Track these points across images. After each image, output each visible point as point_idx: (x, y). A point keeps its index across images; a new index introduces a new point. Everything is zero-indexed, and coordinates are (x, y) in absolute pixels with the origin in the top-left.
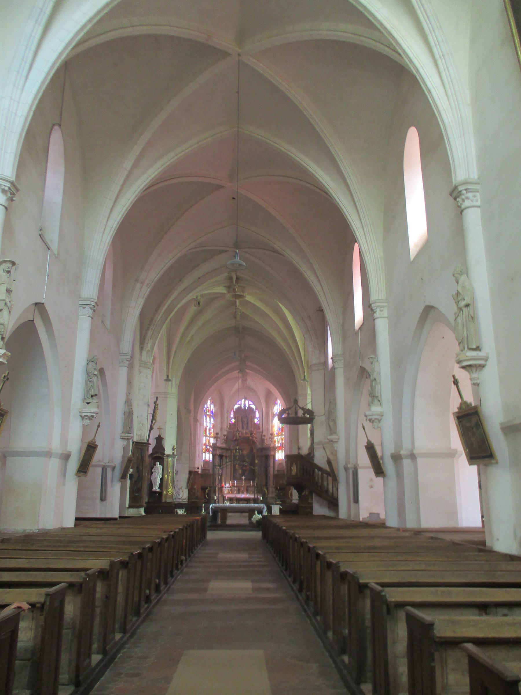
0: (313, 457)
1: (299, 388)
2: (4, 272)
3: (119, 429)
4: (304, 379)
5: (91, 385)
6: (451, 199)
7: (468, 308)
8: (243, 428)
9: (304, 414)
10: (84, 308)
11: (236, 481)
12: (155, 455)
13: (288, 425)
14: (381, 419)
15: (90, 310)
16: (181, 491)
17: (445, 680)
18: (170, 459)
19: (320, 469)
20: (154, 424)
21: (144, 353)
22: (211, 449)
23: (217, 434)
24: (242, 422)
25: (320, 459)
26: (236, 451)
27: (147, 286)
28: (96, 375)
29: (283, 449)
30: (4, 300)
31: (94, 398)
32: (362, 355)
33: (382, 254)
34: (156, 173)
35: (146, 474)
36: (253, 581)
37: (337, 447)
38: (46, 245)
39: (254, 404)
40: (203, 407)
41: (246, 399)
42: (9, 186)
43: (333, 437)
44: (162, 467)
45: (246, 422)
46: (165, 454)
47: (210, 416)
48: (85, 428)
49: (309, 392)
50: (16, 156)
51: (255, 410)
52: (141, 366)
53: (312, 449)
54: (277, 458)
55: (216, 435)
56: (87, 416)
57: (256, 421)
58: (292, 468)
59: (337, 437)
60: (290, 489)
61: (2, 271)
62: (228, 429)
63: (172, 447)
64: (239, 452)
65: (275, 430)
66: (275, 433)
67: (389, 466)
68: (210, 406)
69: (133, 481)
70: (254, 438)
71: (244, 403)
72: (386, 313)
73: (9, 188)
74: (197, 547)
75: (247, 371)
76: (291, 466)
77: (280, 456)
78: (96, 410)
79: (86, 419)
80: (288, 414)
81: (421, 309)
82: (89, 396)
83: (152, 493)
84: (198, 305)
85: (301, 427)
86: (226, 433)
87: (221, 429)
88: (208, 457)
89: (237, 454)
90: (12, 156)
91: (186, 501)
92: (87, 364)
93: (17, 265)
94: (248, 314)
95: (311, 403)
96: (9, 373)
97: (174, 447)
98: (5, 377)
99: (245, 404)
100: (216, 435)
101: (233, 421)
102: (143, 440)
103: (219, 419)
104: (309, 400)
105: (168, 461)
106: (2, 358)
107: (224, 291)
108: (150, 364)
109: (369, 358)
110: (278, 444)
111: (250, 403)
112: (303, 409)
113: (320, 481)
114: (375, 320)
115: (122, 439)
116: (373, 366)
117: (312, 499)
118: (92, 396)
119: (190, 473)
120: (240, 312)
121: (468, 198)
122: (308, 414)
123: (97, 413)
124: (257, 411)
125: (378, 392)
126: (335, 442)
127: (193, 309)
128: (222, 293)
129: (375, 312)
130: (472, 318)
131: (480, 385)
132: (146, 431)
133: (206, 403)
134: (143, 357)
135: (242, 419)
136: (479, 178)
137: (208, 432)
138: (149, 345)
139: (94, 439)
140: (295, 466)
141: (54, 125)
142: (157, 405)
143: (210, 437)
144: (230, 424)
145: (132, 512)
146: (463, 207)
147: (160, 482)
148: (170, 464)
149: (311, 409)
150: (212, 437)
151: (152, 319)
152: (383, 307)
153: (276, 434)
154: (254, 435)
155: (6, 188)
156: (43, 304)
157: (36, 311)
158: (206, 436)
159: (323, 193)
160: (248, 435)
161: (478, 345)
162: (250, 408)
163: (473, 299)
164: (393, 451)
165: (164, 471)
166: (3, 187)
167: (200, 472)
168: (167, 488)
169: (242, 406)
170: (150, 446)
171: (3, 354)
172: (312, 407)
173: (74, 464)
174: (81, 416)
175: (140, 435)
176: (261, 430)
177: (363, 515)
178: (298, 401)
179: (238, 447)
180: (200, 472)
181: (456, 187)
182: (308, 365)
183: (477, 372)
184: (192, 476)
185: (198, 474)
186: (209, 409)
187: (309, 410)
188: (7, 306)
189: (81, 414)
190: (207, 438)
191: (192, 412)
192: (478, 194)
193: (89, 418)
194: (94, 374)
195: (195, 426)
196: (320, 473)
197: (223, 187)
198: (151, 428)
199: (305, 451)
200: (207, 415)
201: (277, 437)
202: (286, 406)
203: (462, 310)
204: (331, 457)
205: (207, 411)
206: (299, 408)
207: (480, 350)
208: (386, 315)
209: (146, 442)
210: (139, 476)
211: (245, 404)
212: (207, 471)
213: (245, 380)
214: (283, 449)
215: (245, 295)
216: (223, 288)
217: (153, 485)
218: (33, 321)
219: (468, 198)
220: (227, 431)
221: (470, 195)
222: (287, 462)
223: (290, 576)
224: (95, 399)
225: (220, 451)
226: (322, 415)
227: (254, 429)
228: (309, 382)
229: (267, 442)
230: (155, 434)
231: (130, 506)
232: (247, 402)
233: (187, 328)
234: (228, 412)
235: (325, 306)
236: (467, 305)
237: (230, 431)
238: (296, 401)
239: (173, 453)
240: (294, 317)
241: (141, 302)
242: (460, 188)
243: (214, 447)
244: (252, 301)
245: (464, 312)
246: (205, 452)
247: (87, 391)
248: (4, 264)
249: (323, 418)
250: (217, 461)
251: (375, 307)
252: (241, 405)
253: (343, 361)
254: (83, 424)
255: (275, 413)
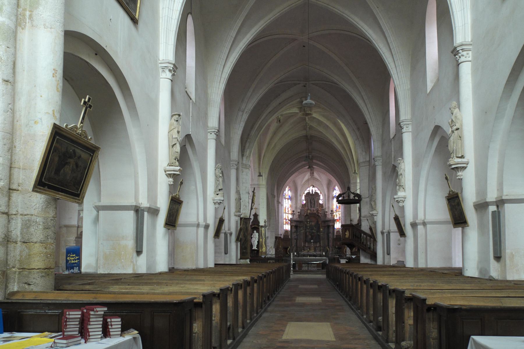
0: (361, 225)
1: (351, 178)
2: (175, 121)
3: (233, 210)
4: (355, 173)
5: (218, 183)
6: (452, 55)
7: (458, 130)
8: (311, 207)
9: (354, 197)
10: (211, 134)
11: (307, 243)
12: (253, 226)
13: (344, 205)
14: (405, 200)
15: (214, 135)
16: (271, 249)
17: (410, 314)
18: (263, 229)
19: (365, 233)
20: (253, 206)
21: (244, 158)
22: (289, 222)
23: (293, 211)
24: (311, 203)
25: (365, 227)
26: (307, 223)
27: (246, 113)
28: (221, 177)
29: (340, 221)
30: (177, 138)
31: (220, 191)
32: (394, 157)
33: (409, 87)
34: (252, 37)
35: (249, 237)
36: (321, 297)
37: (376, 219)
38: (190, 98)
39: (319, 190)
40: (283, 193)
41: (313, 187)
42: (172, 67)
43: (374, 212)
44: (258, 234)
45: (313, 203)
46: (259, 225)
47: (288, 199)
48: (216, 210)
49: (358, 181)
50: (174, 46)
51: (320, 195)
52: (243, 168)
53: (360, 220)
54: (335, 227)
55: (292, 213)
56: (217, 202)
57: (321, 202)
58: (346, 233)
59: (376, 212)
60: (345, 248)
61: (174, 121)
62: (301, 208)
63: (264, 221)
64: (310, 223)
65: (334, 208)
66: (334, 210)
67: (408, 230)
68: (288, 192)
69: (242, 243)
70: (320, 214)
71: (311, 189)
72: (410, 128)
73: (173, 68)
74: (286, 282)
75: (314, 167)
76: (345, 232)
77: (338, 226)
78: (222, 198)
79: (217, 204)
80: (343, 197)
81: (432, 128)
82: (218, 190)
83: (253, 251)
84: (279, 122)
85: (352, 205)
86: (299, 211)
87: (296, 208)
88: (287, 227)
89: (308, 225)
90: (172, 46)
91: (274, 256)
92: (215, 170)
93: (181, 116)
94: (315, 126)
95: (359, 189)
96: (182, 180)
97: (265, 220)
98: (181, 182)
99: (312, 190)
100: (292, 213)
101: (304, 202)
102: (247, 216)
103: (294, 201)
104: (358, 187)
105: (262, 230)
106: (179, 171)
107: (297, 111)
108: (249, 166)
109: (398, 160)
110: (336, 217)
111: (316, 189)
112: (353, 193)
113: (365, 241)
114: (403, 134)
115: (235, 216)
116: (400, 166)
117: (360, 254)
118: (220, 190)
119: (276, 238)
120: (309, 126)
121: (463, 55)
122: (357, 197)
123: (223, 201)
124: (321, 194)
125: (403, 183)
126: (375, 215)
127: (274, 125)
128: (296, 113)
129: (403, 128)
130: (460, 137)
131: (463, 179)
132: (248, 210)
133: (285, 190)
134: (244, 161)
135: (310, 200)
136: (471, 41)
137: (287, 210)
138: (247, 153)
139: (222, 216)
140: (348, 232)
141: (188, 14)
142: (255, 193)
143: (288, 214)
144: (302, 204)
145: (242, 261)
146: (460, 61)
147: (257, 244)
148: (263, 232)
149: (359, 194)
150: (290, 214)
151: (249, 135)
152: (408, 124)
153: (335, 210)
154: (320, 212)
155: (171, 69)
156: (190, 135)
157: (186, 140)
158: (286, 213)
159: (368, 42)
160: (315, 212)
161: (463, 155)
162: (316, 193)
163: (462, 125)
164: (412, 221)
165: (260, 237)
166: (169, 68)
167: (282, 238)
168: (262, 248)
169: (311, 192)
170: (251, 220)
171: (179, 170)
172: (360, 193)
173: (211, 231)
174: (214, 202)
175: (245, 213)
176: (324, 208)
177: (393, 262)
178: (350, 188)
179: (308, 220)
180: (282, 238)
181: (455, 48)
182: (357, 161)
183: (461, 172)
184: (277, 240)
185: (281, 239)
186: (287, 194)
187: (358, 194)
188: (178, 141)
189: (214, 201)
190: (286, 214)
191: (276, 197)
192: (470, 52)
193: (219, 204)
194: (220, 176)
195: (278, 206)
196: (365, 236)
197: (297, 39)
198: (252, 209)
199: (355, 222)
200: (286, 198)
201: (336, 213)
202: (342, 191)
203: (454, 133)
204: (372, 226)
205: (286, 196)
206: (351, 193)
207: (464, 158)
208: (410, 130)
209: (249, 217)
210: (245, 240)
211: (312, 190)
212: (287, 237)
213: (312, 174)
214: (340, 221)
215: (312, 113)
216: (297, 109)
217: (252, 246)
218: (185, 145)
219: (463, 55)
220: (300, 209)
221: (465, 53)
222: (342, 229)
223: (344, 295)
224: (221, 192)
225: (296, 223)
226: (367, 198)
227: (319, 208)
228: (358, 175)
229: (329, 217)
230: (253, 212)
231: (241, 259)
232: (314, 189)
233: (272, 138)
234: (300, 196)
235: (369, 121)
236: (457, 129)
237: (302, 209)
238: (349, 189)
239: (265, 225)
240: (348, 129)
241: (242, 125)
242: (458, 49)
243: (291, 220)
244: (317, 117)
245: (455, 133)
246: (285, 224)
247: (216, 187)
248: (174, 116)
249: (368, 199)
250: (294, 230)
251: (402, 124)
252: (309, 190)
253: (381, 161)
254: (215, 208)
255: (334, 196)
